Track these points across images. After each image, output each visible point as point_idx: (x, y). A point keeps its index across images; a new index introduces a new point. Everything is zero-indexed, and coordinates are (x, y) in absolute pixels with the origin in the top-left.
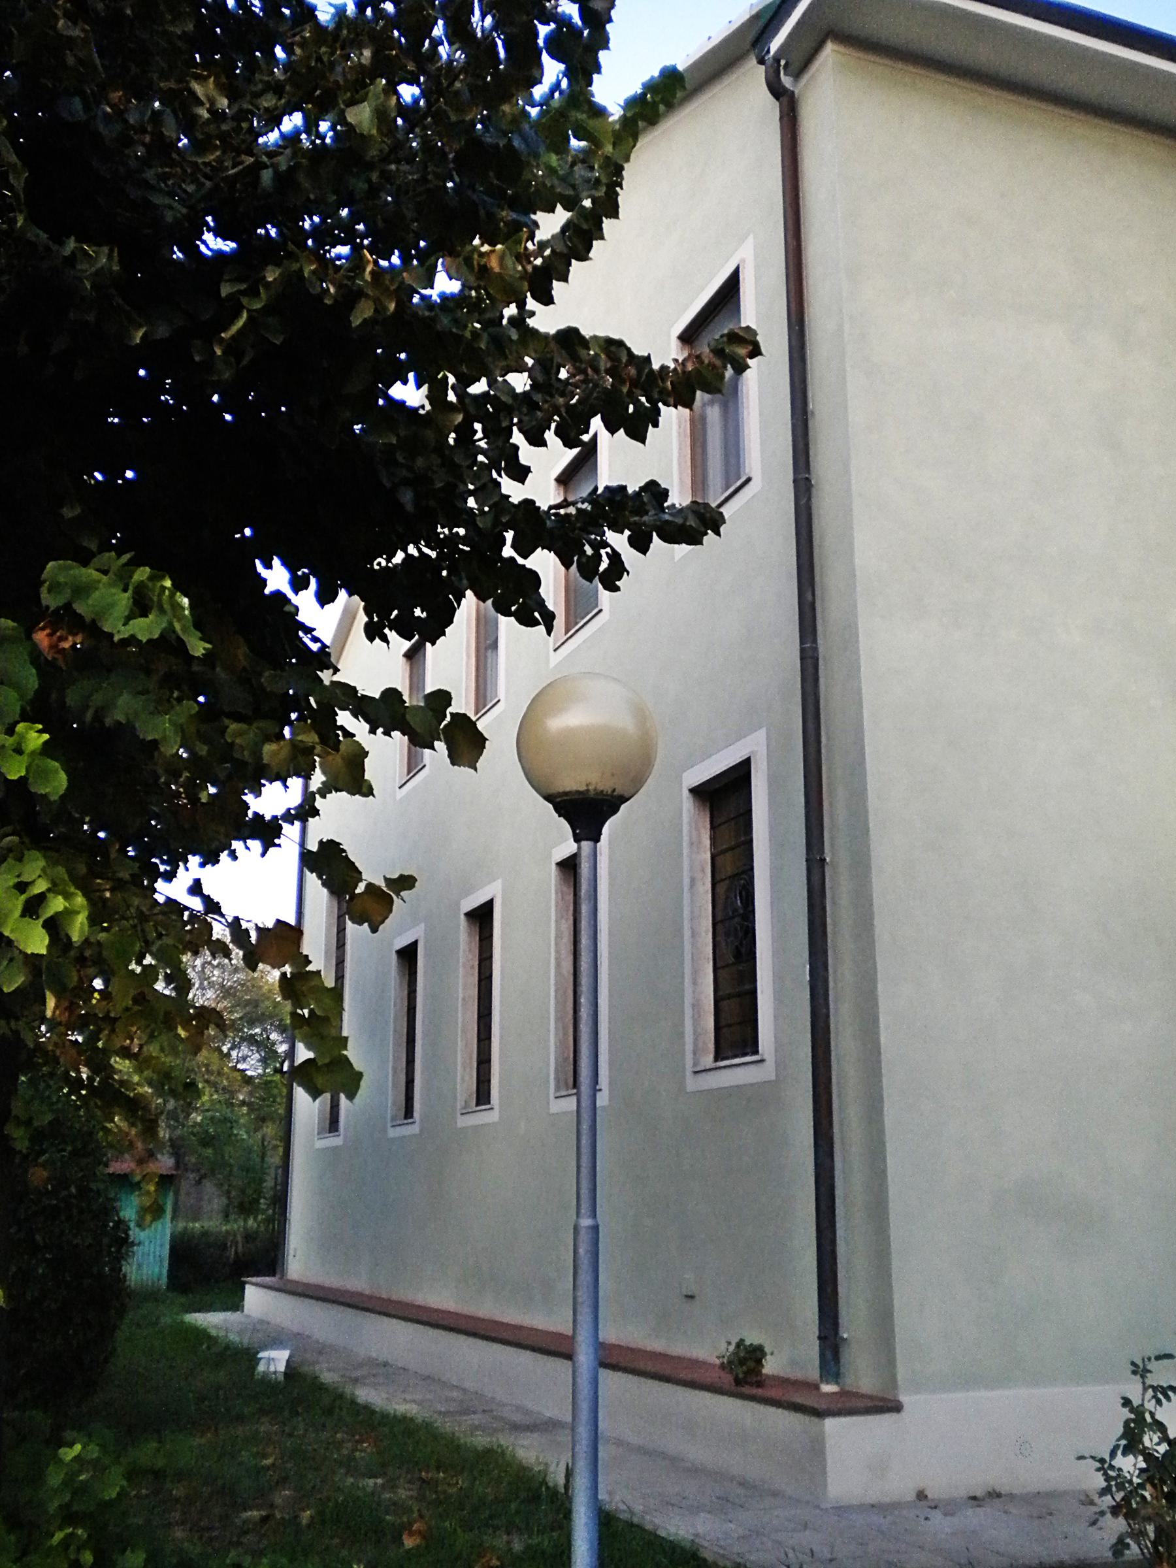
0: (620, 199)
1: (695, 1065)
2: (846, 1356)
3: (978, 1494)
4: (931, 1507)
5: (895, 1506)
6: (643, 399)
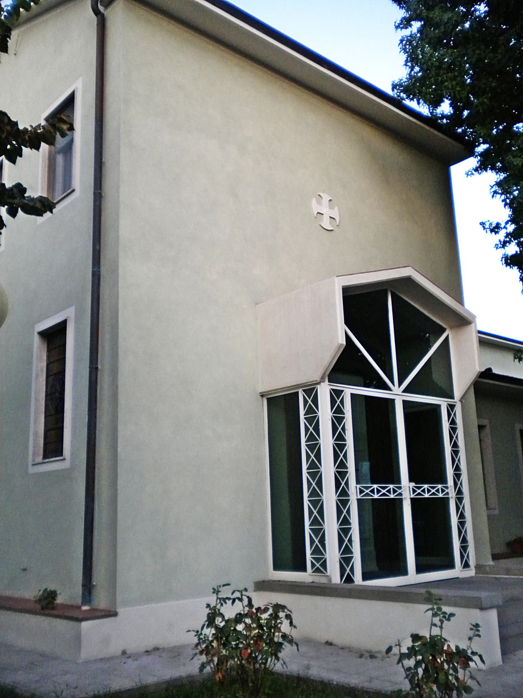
0: (8, 44)
1: (33, 460)
2: (95, 592)
3: (149, 649)
4: (127, 658)
5: (112, 658)
6: (14, 142)
